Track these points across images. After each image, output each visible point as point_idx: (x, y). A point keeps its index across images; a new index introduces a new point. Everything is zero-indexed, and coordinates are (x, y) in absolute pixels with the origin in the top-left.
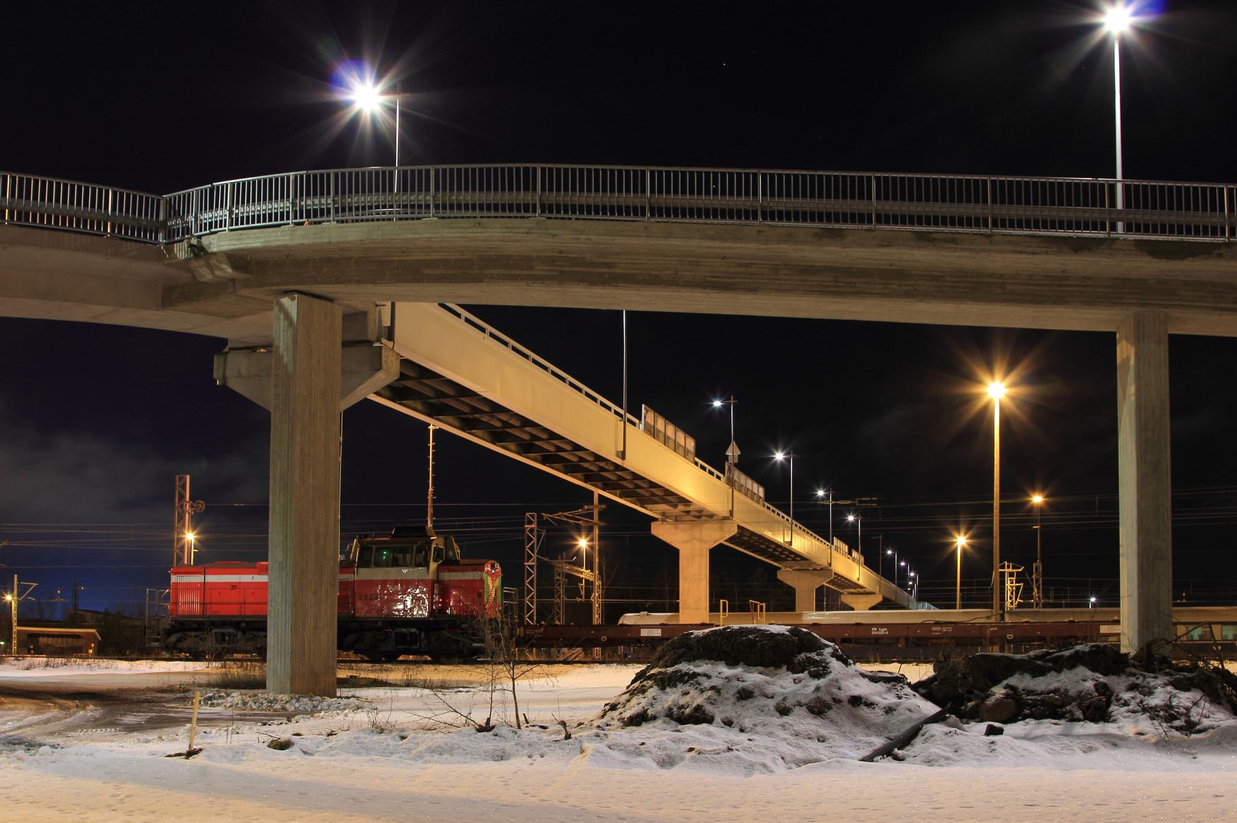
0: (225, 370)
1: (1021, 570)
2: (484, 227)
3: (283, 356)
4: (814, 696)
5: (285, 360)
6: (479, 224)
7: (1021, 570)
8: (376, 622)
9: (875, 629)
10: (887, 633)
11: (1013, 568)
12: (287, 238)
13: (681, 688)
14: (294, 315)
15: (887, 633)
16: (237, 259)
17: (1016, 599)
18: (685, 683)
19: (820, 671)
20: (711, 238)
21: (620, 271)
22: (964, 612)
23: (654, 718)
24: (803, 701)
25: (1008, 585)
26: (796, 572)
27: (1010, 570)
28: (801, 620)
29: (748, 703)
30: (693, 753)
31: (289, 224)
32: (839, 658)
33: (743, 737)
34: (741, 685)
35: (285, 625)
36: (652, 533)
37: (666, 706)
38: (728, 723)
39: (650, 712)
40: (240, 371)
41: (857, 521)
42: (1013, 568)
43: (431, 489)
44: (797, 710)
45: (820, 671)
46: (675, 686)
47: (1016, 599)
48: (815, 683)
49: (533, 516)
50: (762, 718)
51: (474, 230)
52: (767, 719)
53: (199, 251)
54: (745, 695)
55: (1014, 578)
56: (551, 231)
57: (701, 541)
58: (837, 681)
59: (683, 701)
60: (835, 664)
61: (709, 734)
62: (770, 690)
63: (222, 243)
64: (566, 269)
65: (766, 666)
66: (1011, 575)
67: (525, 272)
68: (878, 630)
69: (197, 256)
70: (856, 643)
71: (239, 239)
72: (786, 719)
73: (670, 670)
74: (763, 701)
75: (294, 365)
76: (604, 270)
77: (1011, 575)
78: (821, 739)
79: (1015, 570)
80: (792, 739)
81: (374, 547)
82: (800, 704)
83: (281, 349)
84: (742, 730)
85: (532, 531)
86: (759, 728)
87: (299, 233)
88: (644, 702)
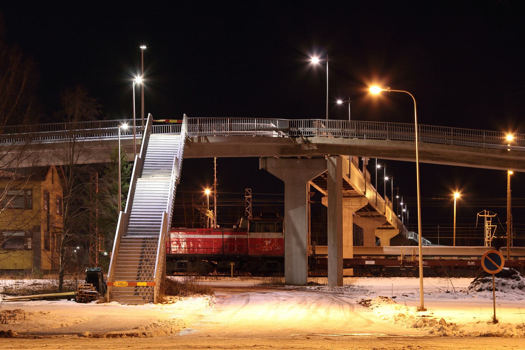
0: (266, 165)
1: (494, 216)
2: (405, 144)
3: (331, 177)
4: (519, 285)
5: (333, 178)
6: (403, 143)
7: (494, 216)
8: (258, 258)
9: (469, 262)
10: (474, 264)
11: (489, 215)
12: (341, 142)
13: (488, 283)
14: (335, 163)
15: (474, 264)
16: (318, 145)
17: (492, 236)
18: (489, 282)
19: (518, 279)
20: (471, 151)
21: (441, 157)
22: (476, 248)
23: (484, 290)
24: (517, 286)
25: (487, 225)
26: (363, 218)
27: (488, 216)
28: (383, 251)
29: (505, 286)
30: (498, 297)
31: (340, 137)
32: (522, 276)
33: (506, 294)
34: (502, 282)
35: (335, 264)
36: (322, 203)
37: (486, 287)
38: (501, 291)
39: (483, 288)
40: (272, 166)
41: (390, 180)
42: (489, 215)
43: (215, 180)
44: (516, 288)
45: (518, 279)
46: (486, 282)
47: (492, 236)
48: (518, 282)
49: (249, 191)
50: (509, 290)
51: (402, 144)
52: (510, 290)
53: (307, 142)
54: (503, 284)
55: (490, 222)
56: (425, 146)
57: (349, 208)
58: (523, 281)
59: (490, 286)
60: (521, 277)
61: (498, 293)
62: (509, 283)
63: (317, 141)
64: (425, 155)
65: (506, 278)
66: (488, 219)
67: (413, 155)
68: (470, 263)
69: (306, 143)
70: (460, 268)
71: (323, 140)
72: (514, 290)
73: (484, 278)
74: (508, 286)
75: (336, 180)
76: (436, 156)
77: (488, 219)
78: (523, 295)
79: (490, 216)
80: (517, 294)
81: (256, 223)
82: (516, 287)
83: (331, 174)
84: (505, 292)
85: (249, 199)
86: (509, 292)
87: (345, 141)
88: (480, 286)
